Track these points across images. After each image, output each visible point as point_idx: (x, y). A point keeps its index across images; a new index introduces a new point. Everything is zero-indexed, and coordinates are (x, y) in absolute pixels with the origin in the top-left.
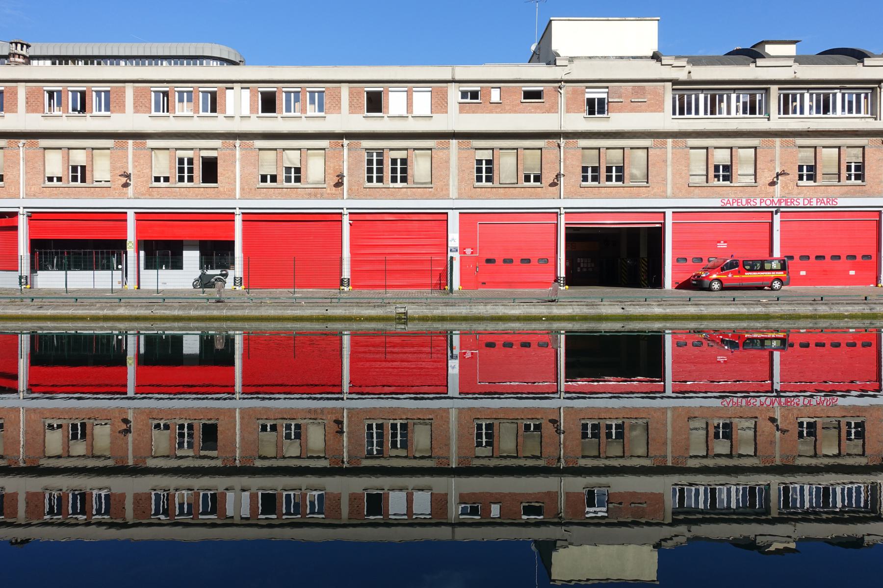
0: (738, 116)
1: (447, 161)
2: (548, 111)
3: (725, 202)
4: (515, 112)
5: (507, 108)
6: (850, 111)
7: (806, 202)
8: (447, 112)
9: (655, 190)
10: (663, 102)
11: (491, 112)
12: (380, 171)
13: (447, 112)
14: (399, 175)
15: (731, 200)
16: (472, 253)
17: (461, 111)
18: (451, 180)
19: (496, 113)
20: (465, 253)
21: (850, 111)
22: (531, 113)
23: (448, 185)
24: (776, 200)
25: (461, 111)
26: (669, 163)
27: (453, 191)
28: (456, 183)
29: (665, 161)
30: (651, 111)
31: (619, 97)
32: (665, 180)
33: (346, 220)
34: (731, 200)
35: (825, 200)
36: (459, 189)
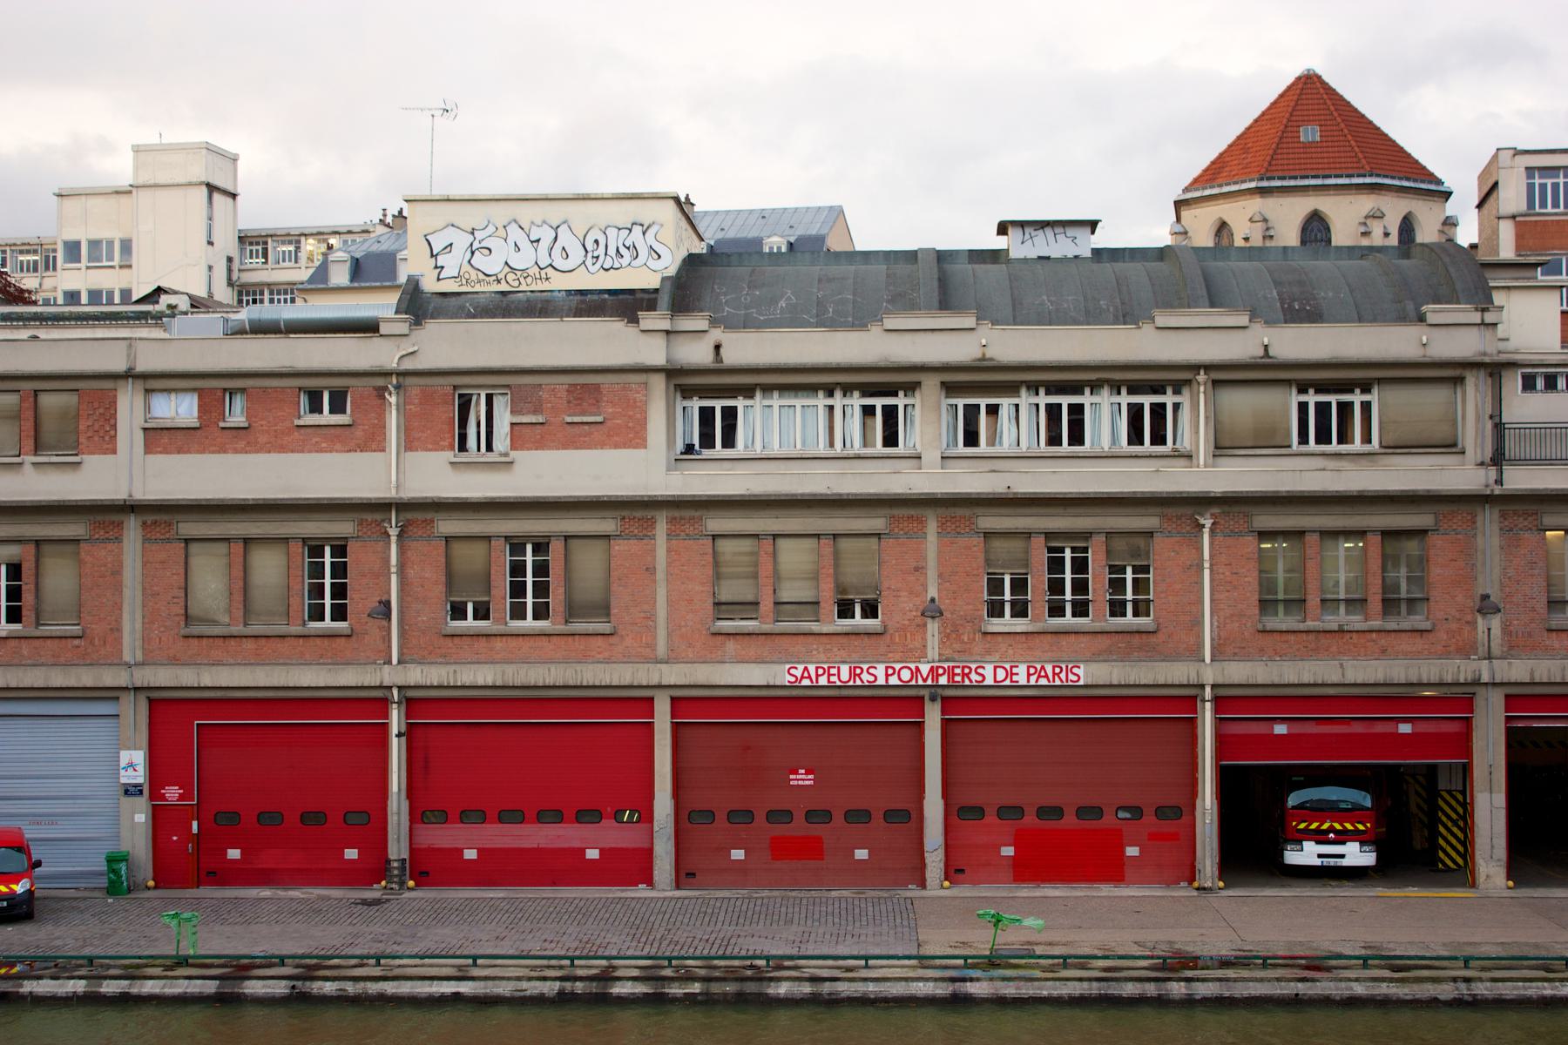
0: (869, 451)
1: (117, 572)
2: (363, 448)
3: (798, 673)
4: (282, 449)
5: (263, 439)
6: (1323, 437)
7: (1001, 674)
8: (114, 452)
9: (628, 641)
10: (643, 423)
11: (223, 450)
12: (1080, 587)
13: (114, 452)
14: (328, 601)
15: (812, 668)
16: (181, 797)
17: (149, 449)
18: (126, 617)
19: (236, 451)
20: (163, 798)
21: (1323, 437)
22: (321, 451)
23: (119, 630)
24: (925, 668)
25: (149, 449)
26: (660, 575)
27: (130, 648)
28: (139, 626)
29: (651, 570)
30: (616, 446)
31: (535, 412)
32: (651, 617)
33: (662, 709)
34: (812, 668)
35: (1049, 668)
36: (146, 640)
